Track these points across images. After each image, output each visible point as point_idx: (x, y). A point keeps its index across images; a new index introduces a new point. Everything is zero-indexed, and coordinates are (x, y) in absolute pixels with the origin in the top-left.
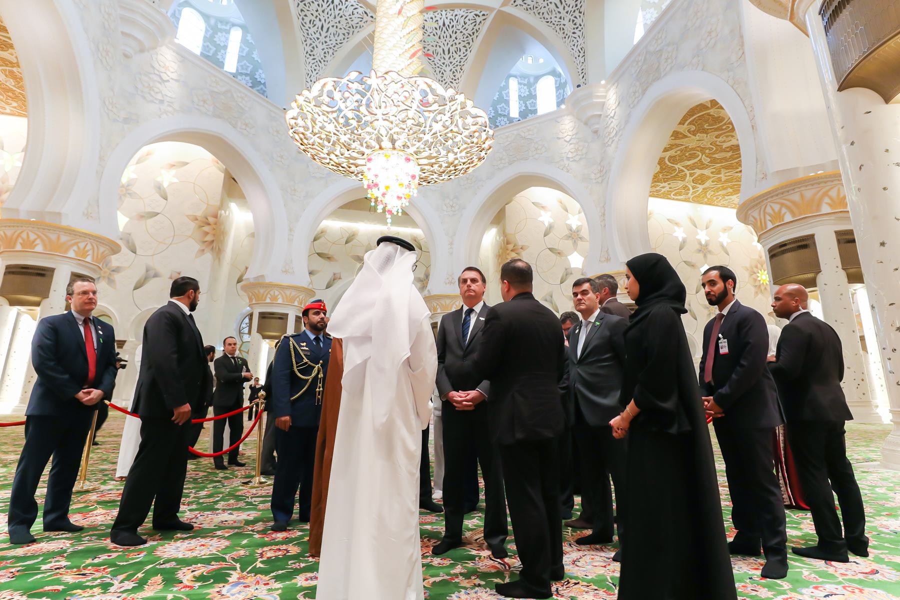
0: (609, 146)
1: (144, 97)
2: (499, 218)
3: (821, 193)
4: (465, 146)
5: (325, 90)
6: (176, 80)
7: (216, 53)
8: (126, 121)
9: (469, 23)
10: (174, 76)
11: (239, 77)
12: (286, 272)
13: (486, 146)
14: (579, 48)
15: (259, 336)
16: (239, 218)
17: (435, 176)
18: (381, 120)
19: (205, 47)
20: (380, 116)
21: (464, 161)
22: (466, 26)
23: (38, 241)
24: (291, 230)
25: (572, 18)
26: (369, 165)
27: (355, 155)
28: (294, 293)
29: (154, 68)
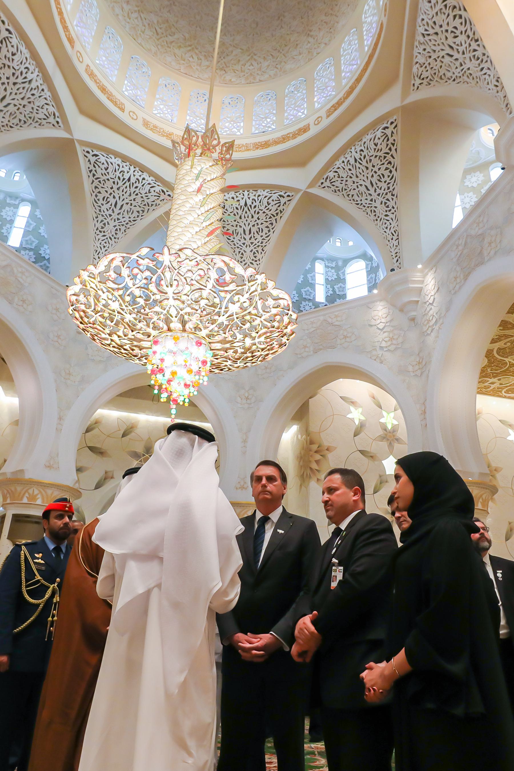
5: (113, 265)
9: (272, 203)
11: (23, 252)
12: (49, 467)
13: (288, 331)
14: (392, 230)
17: (230, 362)
18: (171, 299)
20: (170, 295)
21: (263, 346)
22: (270, 207)
24: (60, 419)
27: (140, 336)
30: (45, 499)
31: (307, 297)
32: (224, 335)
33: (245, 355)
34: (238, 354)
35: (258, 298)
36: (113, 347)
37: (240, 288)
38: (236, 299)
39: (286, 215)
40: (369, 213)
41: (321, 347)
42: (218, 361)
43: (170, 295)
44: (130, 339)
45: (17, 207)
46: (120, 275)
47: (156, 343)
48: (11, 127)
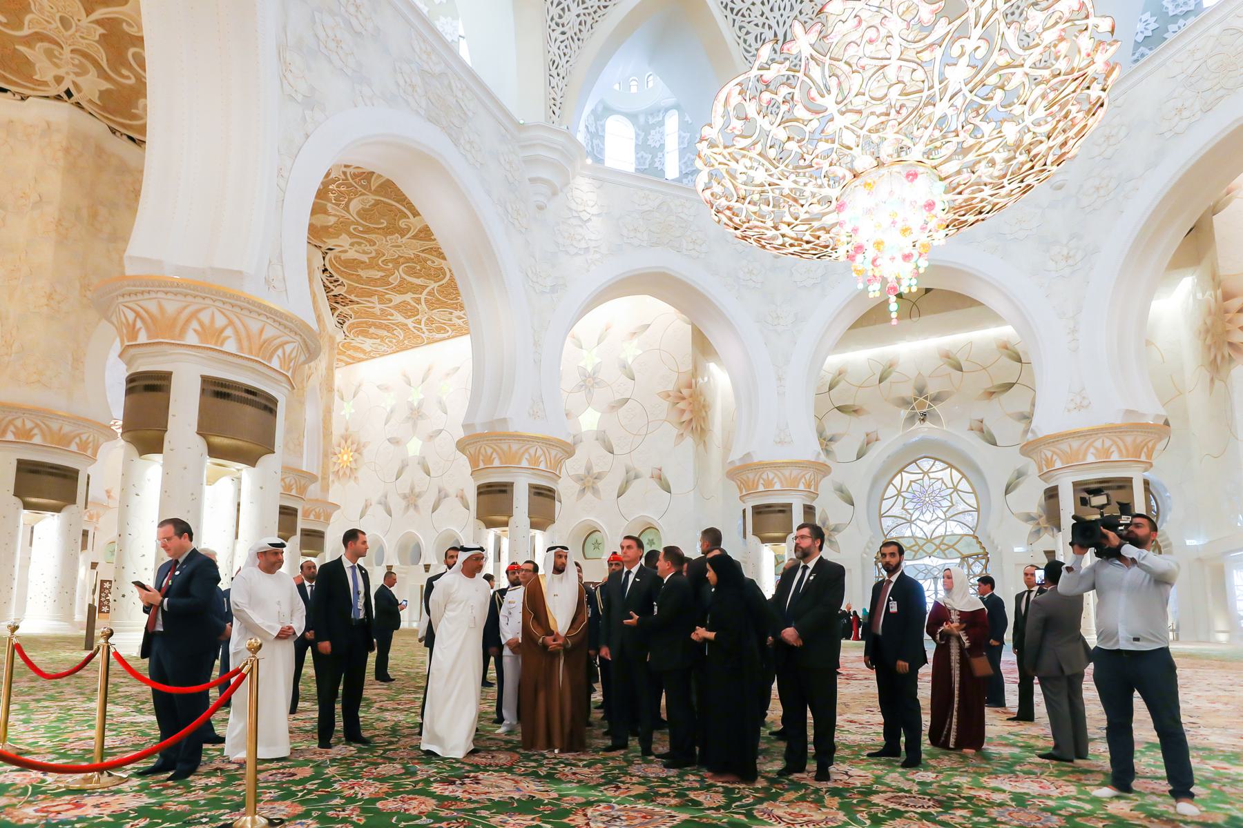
1: (567, 253)
2: (1197, 242)
4: (1039, 90)
5: (731, 109)
6: (599, 215)
7: (652, 162)
8: (554, 289)
10: (595, 210)
11: (685, 181)
12: (781, 442)
13: (1099, 67)
15: (757, 540)
16: (719, 380)
17: (988, 191)
18: (837, 116)
19: (639, 160)
20: (833, 109)
21: (1046, 128)
23: (36, 431)
24: (780, 379)
26: (843, 216)
27: (816, 209)
28: (270, 332)
29: (570, 209)
30: (245, 344)
31: (1178, 11)
32: (956, 140)
33: (1014, 162)
34: (998, 167)
35: (1003, 24)
36: (791, 245)
37: (958, 22)
38: (956, 51)
41: (1222, 92)
42: (965, 195)
43: (833, 109)
44: (807, 221)
45: (661, 124)
46: (746, 118)
47: (840, 208)
48: (605, 7)
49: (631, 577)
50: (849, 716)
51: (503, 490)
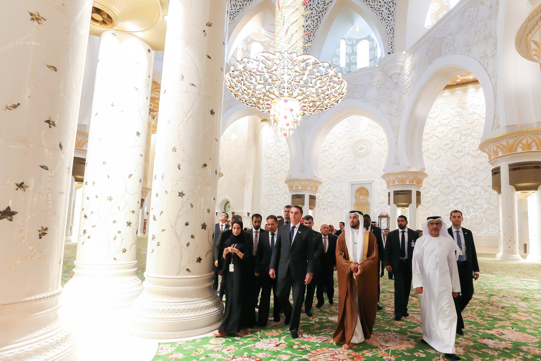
0: (405, 94)
3: (517, 141)
9: (321, 3)
14: (391, 27)
22: (319, 5)
25: (388, 7)
39: (328, 12)
40: (378, 14)
49: (296, 231)
50: (410, 309)
51: (302, 197)
